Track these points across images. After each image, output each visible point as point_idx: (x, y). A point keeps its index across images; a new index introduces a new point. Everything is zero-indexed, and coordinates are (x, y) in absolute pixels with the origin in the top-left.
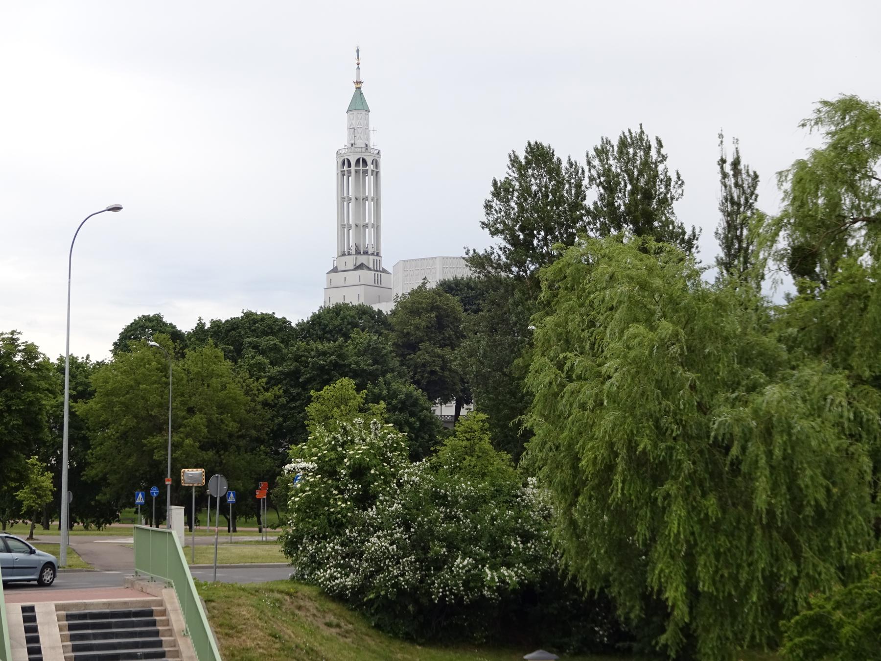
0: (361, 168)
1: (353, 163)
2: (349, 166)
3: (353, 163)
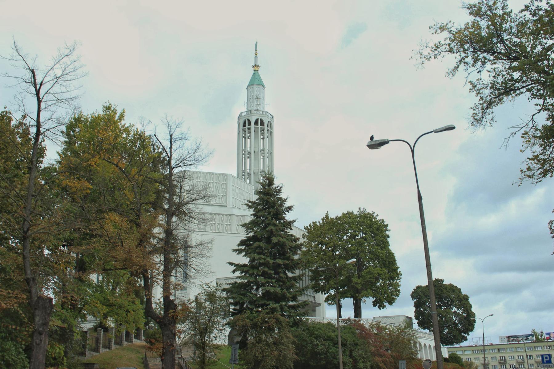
0: (259, 126)
1: (253, 123)
2: (250, 124)
3: (253, 123)
